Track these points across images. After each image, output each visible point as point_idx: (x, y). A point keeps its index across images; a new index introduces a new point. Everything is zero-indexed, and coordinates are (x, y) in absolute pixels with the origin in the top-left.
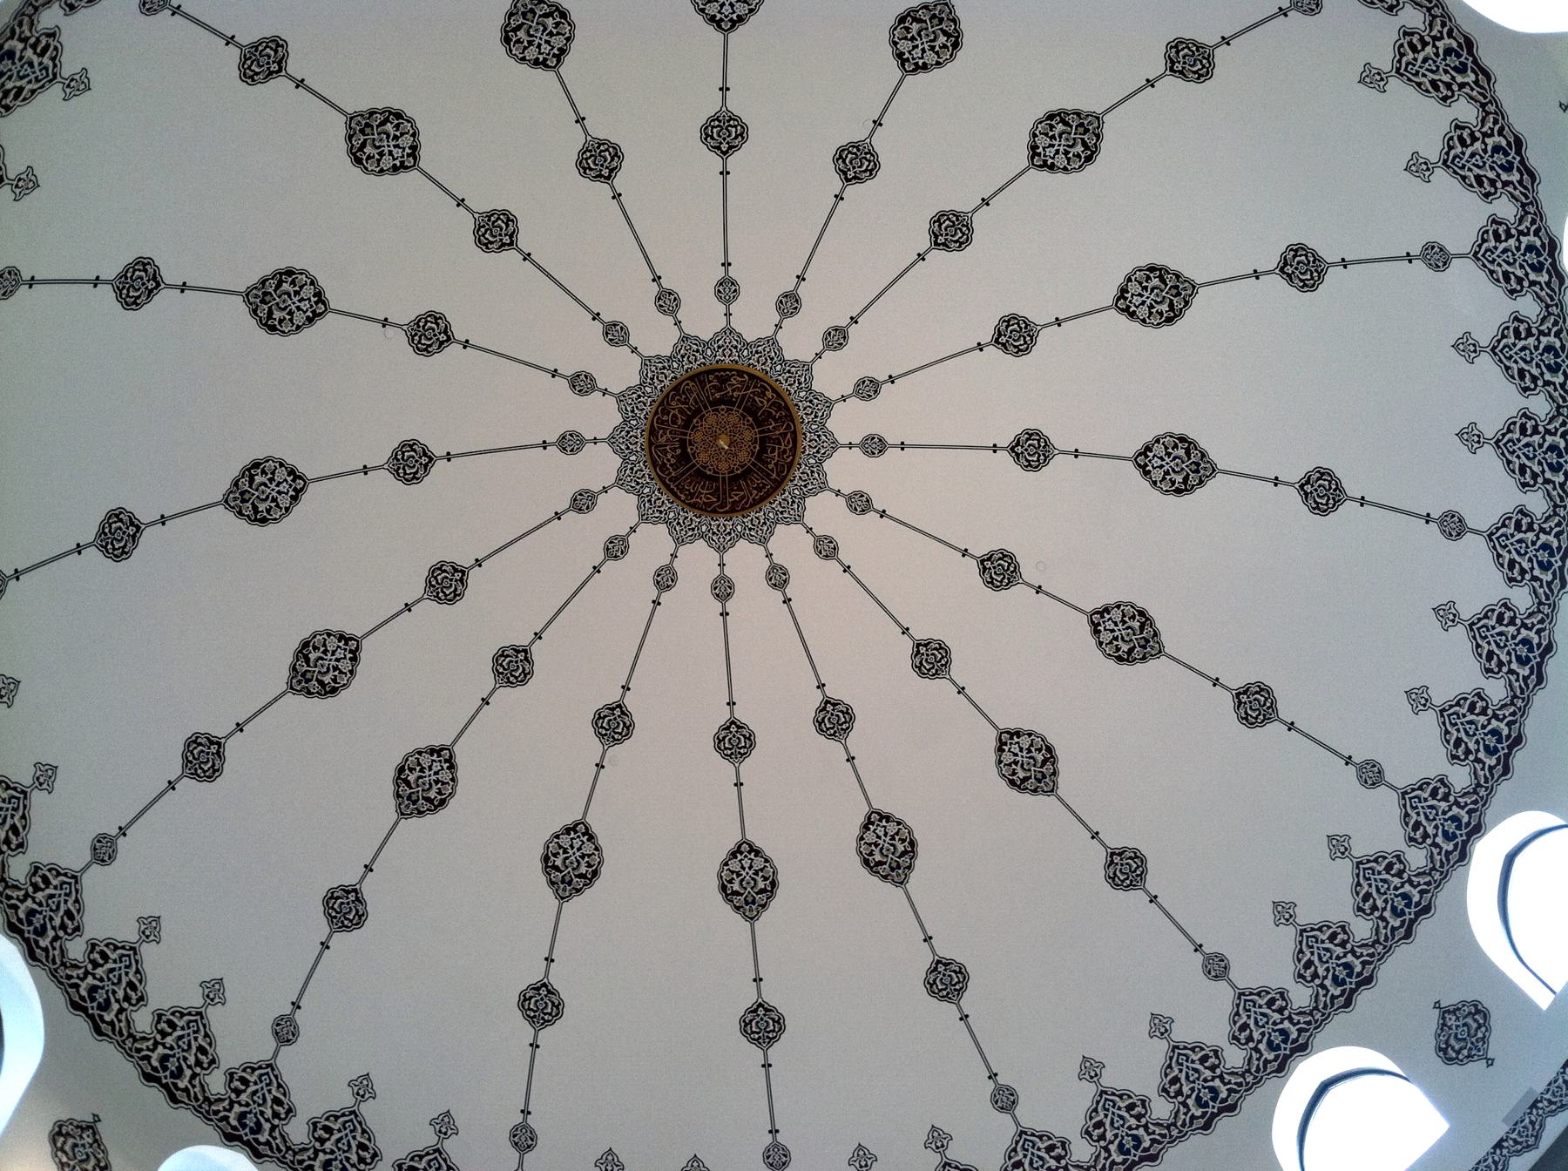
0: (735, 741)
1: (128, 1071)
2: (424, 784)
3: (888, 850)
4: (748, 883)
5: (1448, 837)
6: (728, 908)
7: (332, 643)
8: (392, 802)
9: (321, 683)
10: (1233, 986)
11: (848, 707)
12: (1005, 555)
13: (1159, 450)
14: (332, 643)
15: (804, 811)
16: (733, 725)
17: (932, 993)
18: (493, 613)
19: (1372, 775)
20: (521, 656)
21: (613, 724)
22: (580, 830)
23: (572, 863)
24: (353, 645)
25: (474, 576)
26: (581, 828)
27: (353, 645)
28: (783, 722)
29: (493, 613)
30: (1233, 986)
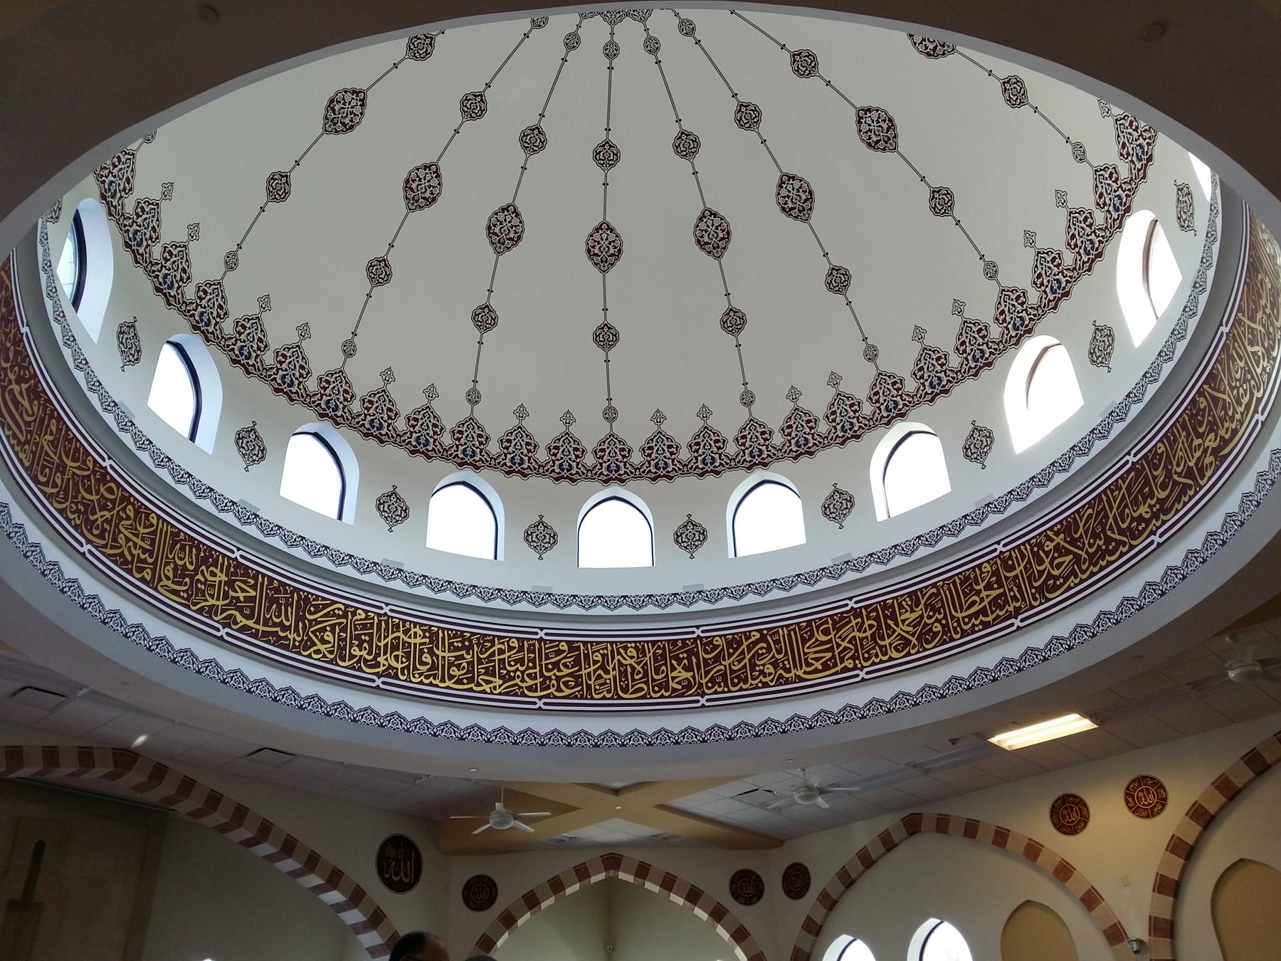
0: (687, 145)
1: (403, 454)
2: (505, 231)
3: (796, 200)
4: (713, 235)
5: (887, 409)
6: (703, 253)
7: (422, 173)
8: (491, 249)
9: (424, 198)
10: (999, 284)
11: (617, 333)
12: (616, 335)
13: (717, 221)
14: (422, 173)
15: (738, 180)
16: (683, 134)
17: (830, 289)
18: (510, 110)
19: (871, 354)
20: (536, 132)
21: (607, 155)
22: (604, 227)
23: (604, 249)
24: (434, 168)
25: (488, 95)
26: (604, 226)
27: (434, 168)
28: (715, 127)
29: (510, 110)
30: (999, 284)
